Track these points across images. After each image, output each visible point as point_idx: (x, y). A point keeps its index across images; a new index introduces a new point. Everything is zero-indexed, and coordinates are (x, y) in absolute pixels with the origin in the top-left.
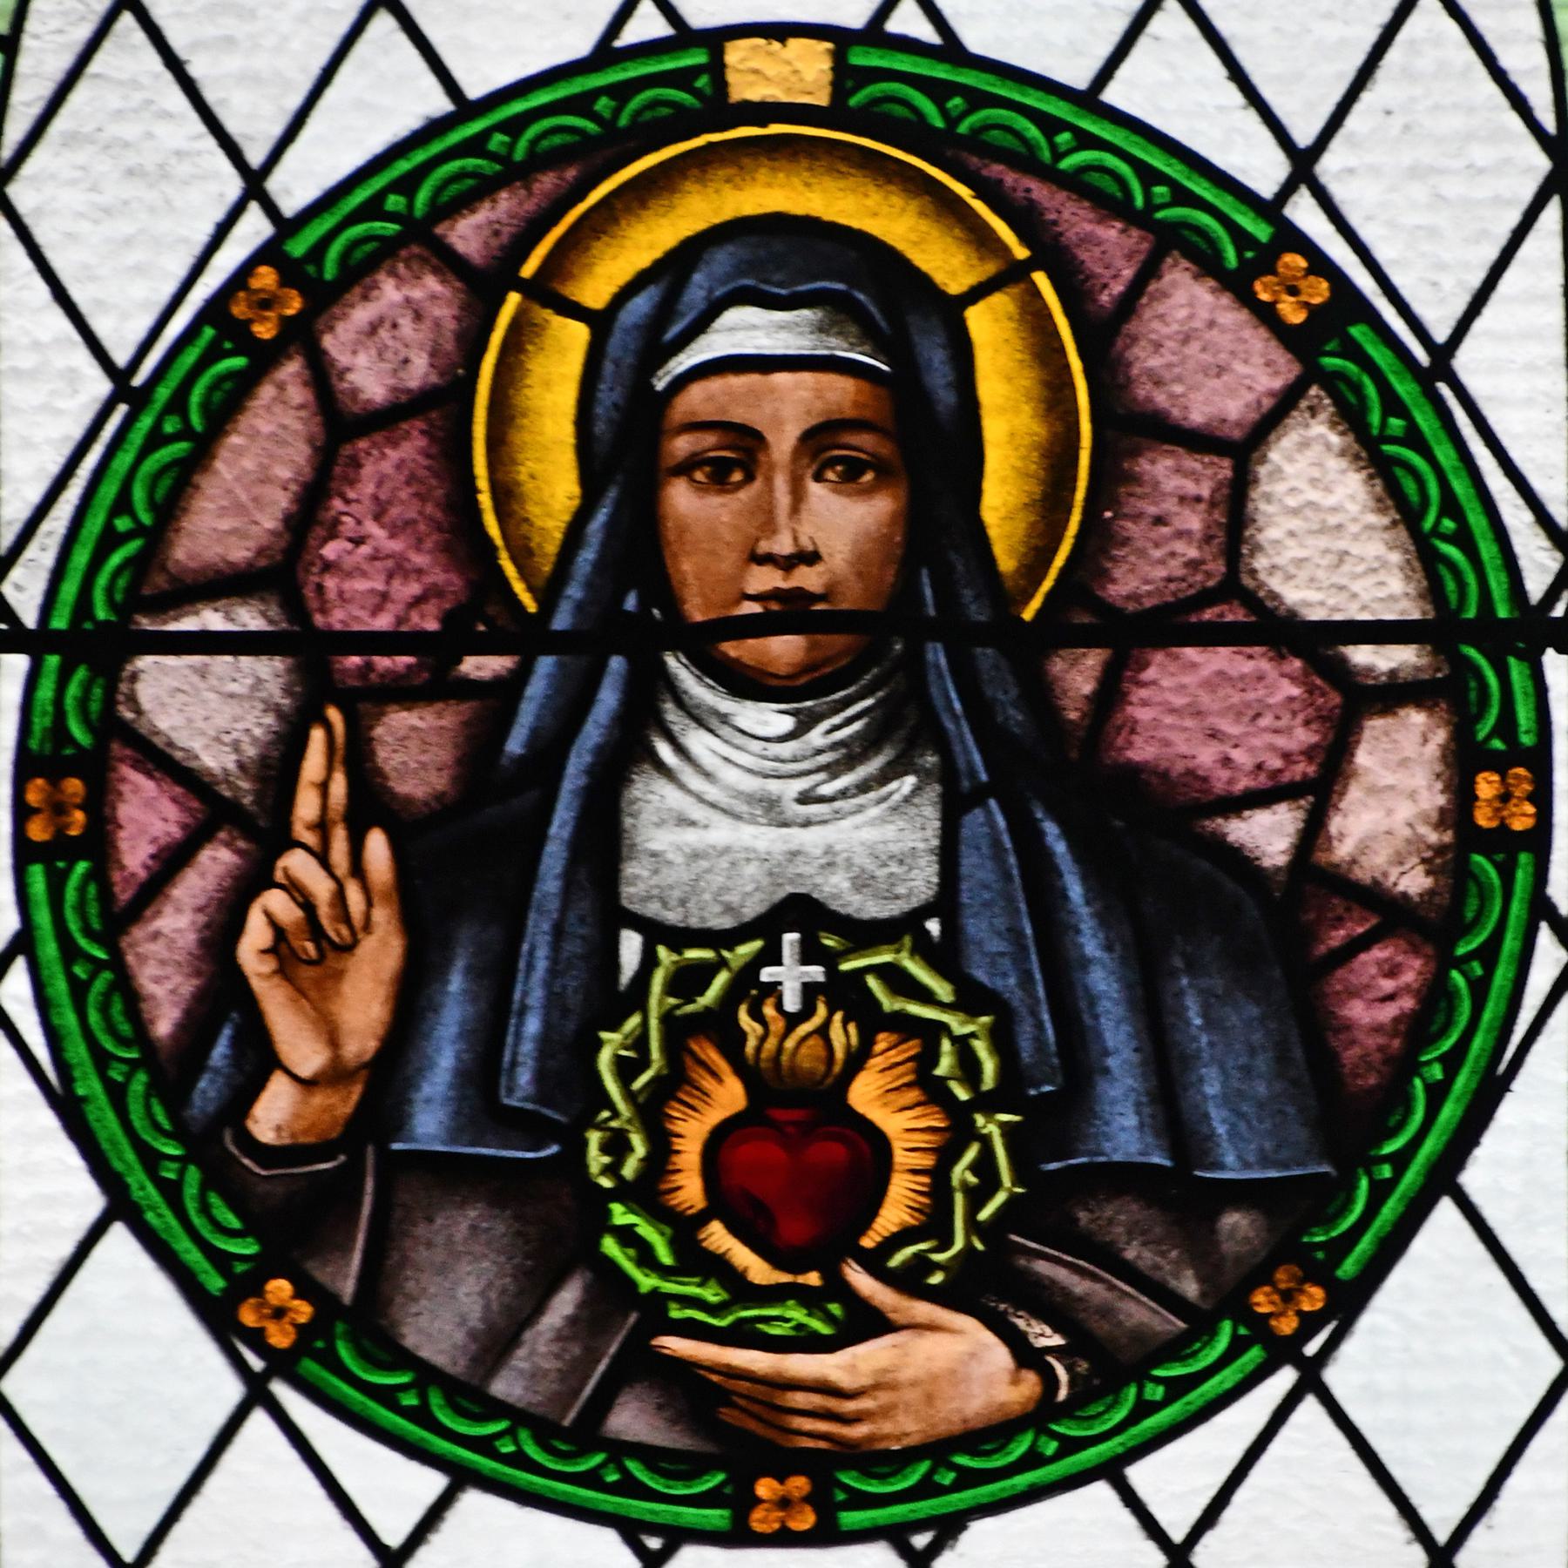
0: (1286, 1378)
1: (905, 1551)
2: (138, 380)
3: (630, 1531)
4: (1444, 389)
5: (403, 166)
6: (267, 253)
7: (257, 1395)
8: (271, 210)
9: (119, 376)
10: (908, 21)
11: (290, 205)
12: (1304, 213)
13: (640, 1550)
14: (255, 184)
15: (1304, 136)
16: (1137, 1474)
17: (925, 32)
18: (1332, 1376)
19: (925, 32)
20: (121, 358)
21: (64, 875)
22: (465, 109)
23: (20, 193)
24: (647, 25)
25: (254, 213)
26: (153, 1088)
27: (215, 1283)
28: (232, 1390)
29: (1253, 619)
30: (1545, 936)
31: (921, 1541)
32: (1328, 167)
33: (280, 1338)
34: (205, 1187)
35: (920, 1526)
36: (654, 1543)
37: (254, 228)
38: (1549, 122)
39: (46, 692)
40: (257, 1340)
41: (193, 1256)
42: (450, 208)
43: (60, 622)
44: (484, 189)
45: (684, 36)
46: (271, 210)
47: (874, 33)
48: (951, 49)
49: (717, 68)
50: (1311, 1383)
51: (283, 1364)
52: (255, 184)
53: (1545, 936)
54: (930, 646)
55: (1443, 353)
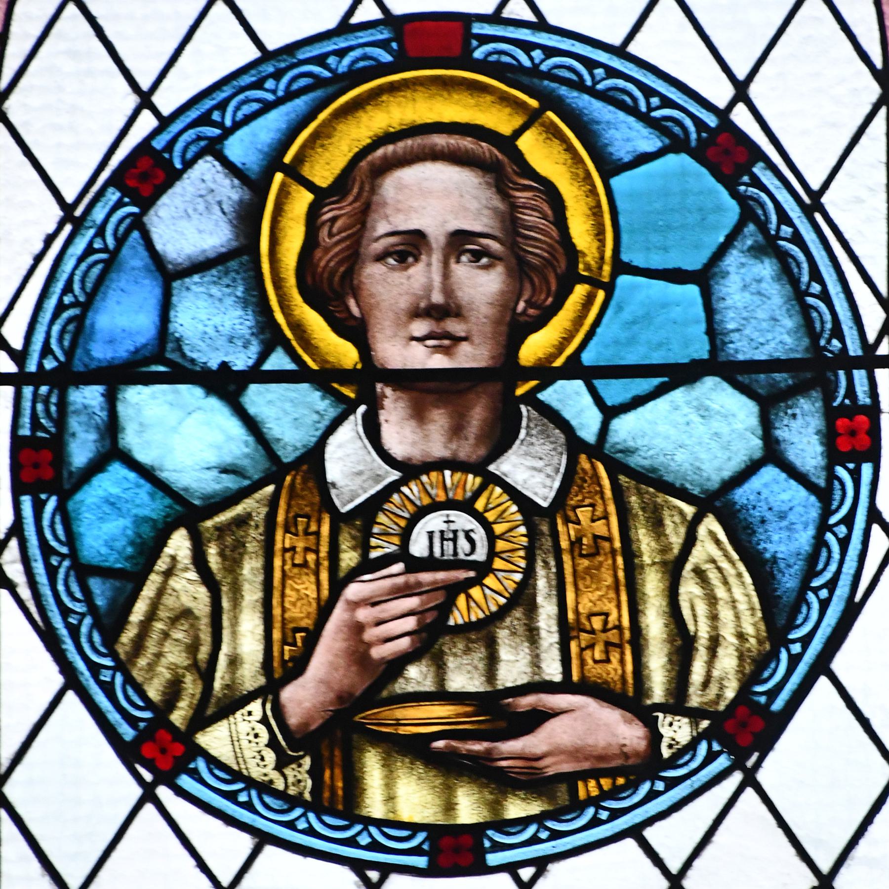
0: (737, 777)
1: (517, 879)
2: (78, 212)
3: (358, 867)
4: (818, 217)
5: (221, 96)
7: (149, 796)
9: (67, 208)
10: (517, 9)
12: (741, 117)
13: (365, 880)
14: (145, 100)
15: (741, 74)
20: (70, 198)
21: (44, 503)
22: (267, 55)
23: (13, 107)
24: (368, 12)
26: (96, 625)
28: (137, 792)
29: (379, 387)
32: (755, 91)
34: (69, 569)
36: (374, 875)
37: (147, 122)
38: (878, 62)
41: (114, 717)
48: (541, 25)
50: (750, 781)
52: (145, 100)
53: (876, 529)
55: (816, 195)
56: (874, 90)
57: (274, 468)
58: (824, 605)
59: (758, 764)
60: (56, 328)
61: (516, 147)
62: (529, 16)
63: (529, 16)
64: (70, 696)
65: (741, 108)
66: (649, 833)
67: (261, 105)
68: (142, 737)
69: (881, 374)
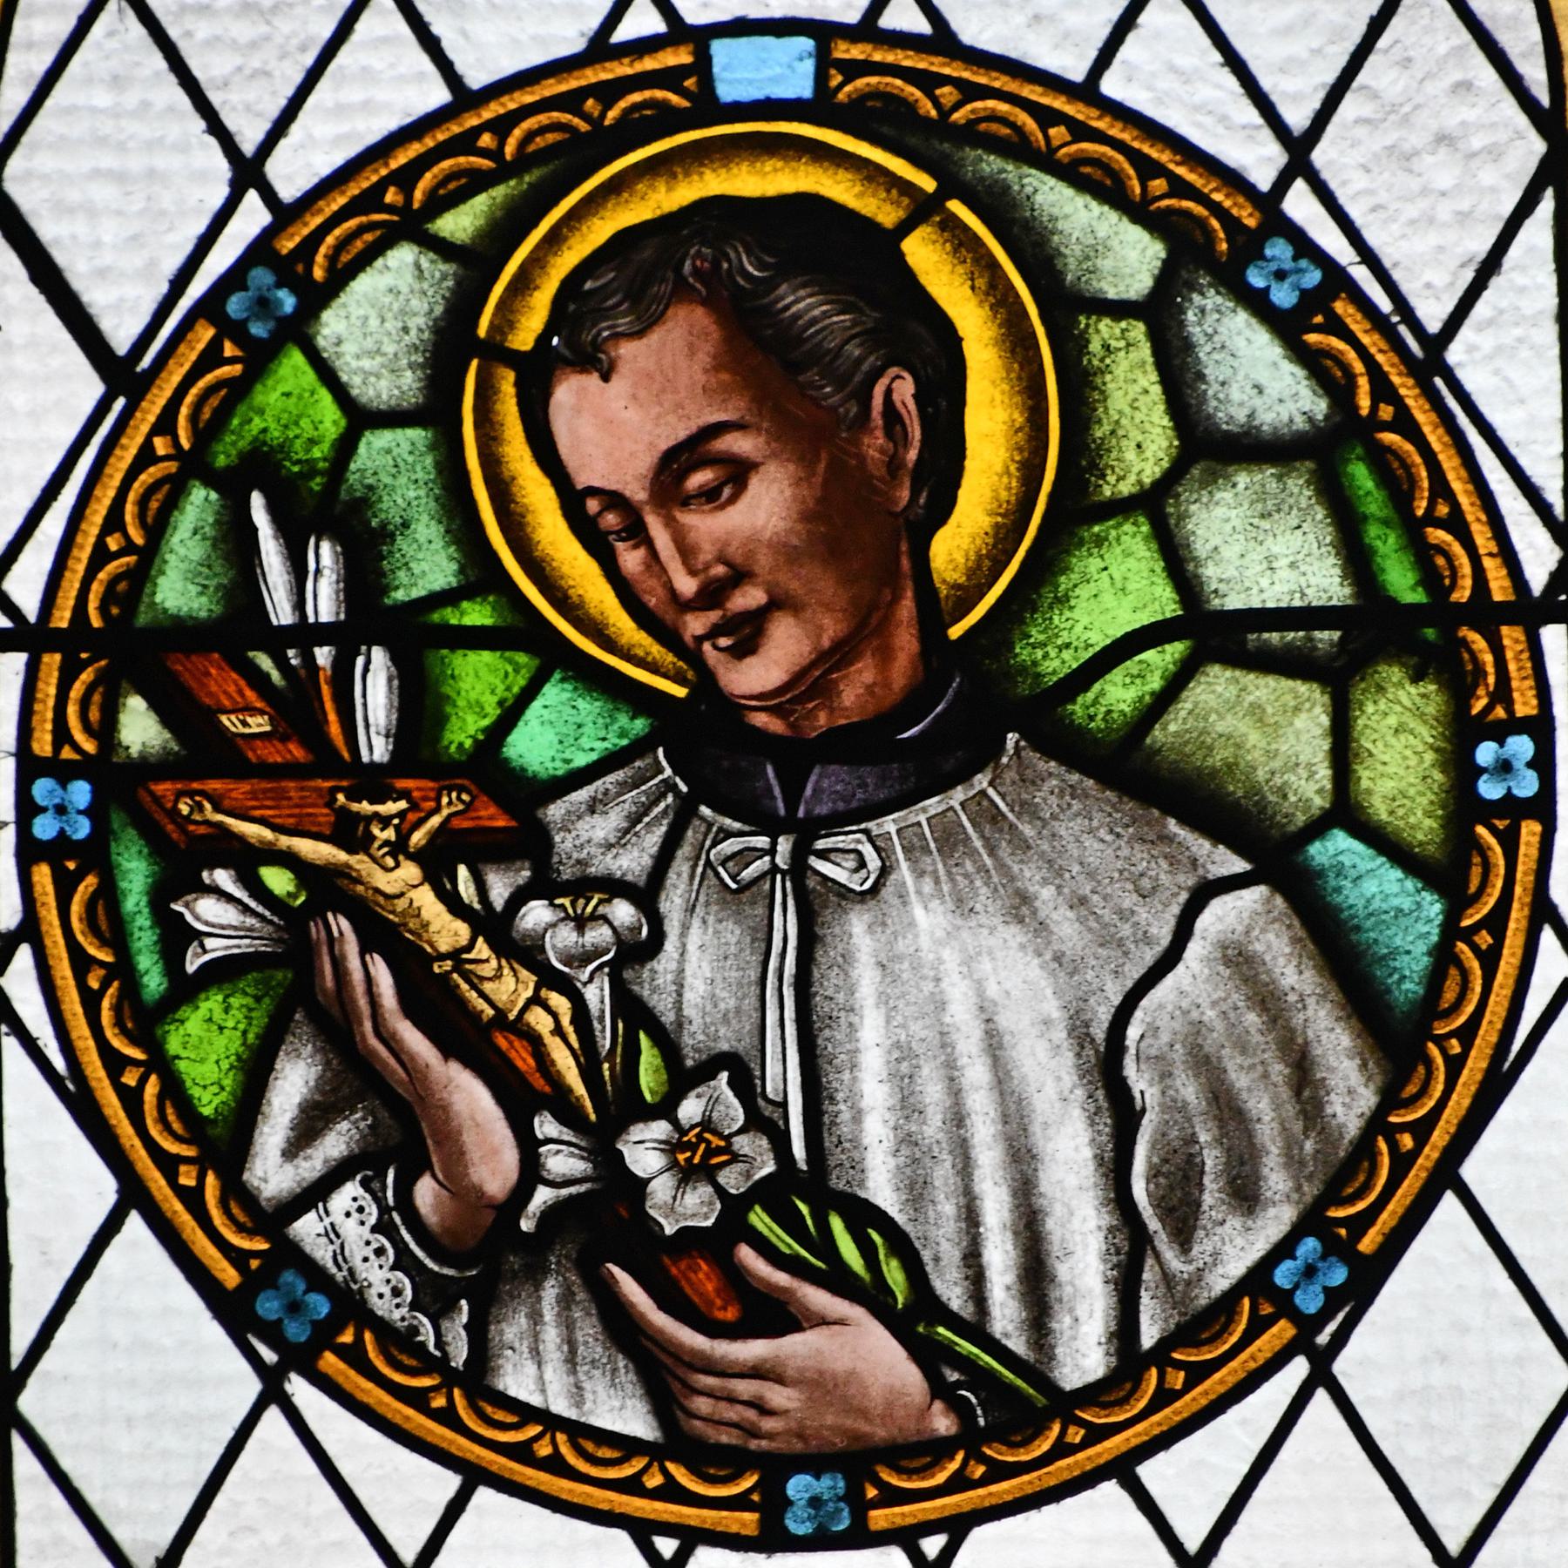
0: (1299, 1368)
1: (915, 1555)
3: (642, 1532)
5: (401, 159)
6: (260, 250)
7: (273, 1394)
8: (269, 196)
10: (903, 16)
11: (288, 192)
12: (1300, 205)
16: (1148, 1472)
17: (920, 24)
18: (1342, 1367)
19: (920, 24)
24: (642, 21)
25: (252, 197)
27: (230, 1276)
28: (252, 1387)
30: (1548, 937)
31: (932, 1546)
33: (296, 1332)
35: (929, 1528)
36: (667, 1546)
37: (252, 217)
39: (48, 689)
40: (272, 1334)
42: (441, 202)
43: (62, 618)
44: (476, 183)
45: (677, 31)
46: (269, 196)
47: (867, 29)
48: (943, 39)
49: (703, 65)
50: (1322, 1377)
51: (302, 1360)
53: (1548, 937)
54: (953, 1430)
56: (1537, 146)
57: (480, 866)
58: (1455, 1066)
59: (1341, 1339)
60: (96, 590)
61: (901, 256)
62: (922, 26)
63: (922, 26)
64: (135, 1223)
65: (1300, 186)
66: (1148, 1472)
67: (480, 940)
68: (254, 1283)
69: (1551, 635)
